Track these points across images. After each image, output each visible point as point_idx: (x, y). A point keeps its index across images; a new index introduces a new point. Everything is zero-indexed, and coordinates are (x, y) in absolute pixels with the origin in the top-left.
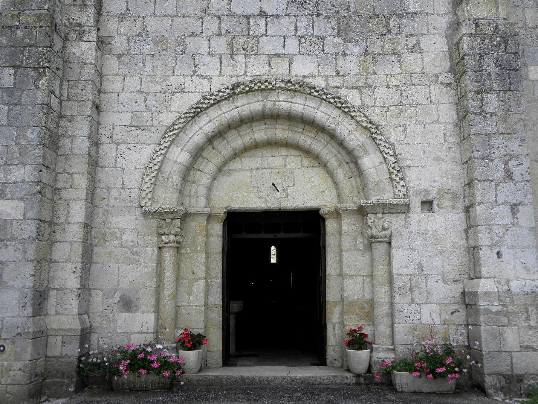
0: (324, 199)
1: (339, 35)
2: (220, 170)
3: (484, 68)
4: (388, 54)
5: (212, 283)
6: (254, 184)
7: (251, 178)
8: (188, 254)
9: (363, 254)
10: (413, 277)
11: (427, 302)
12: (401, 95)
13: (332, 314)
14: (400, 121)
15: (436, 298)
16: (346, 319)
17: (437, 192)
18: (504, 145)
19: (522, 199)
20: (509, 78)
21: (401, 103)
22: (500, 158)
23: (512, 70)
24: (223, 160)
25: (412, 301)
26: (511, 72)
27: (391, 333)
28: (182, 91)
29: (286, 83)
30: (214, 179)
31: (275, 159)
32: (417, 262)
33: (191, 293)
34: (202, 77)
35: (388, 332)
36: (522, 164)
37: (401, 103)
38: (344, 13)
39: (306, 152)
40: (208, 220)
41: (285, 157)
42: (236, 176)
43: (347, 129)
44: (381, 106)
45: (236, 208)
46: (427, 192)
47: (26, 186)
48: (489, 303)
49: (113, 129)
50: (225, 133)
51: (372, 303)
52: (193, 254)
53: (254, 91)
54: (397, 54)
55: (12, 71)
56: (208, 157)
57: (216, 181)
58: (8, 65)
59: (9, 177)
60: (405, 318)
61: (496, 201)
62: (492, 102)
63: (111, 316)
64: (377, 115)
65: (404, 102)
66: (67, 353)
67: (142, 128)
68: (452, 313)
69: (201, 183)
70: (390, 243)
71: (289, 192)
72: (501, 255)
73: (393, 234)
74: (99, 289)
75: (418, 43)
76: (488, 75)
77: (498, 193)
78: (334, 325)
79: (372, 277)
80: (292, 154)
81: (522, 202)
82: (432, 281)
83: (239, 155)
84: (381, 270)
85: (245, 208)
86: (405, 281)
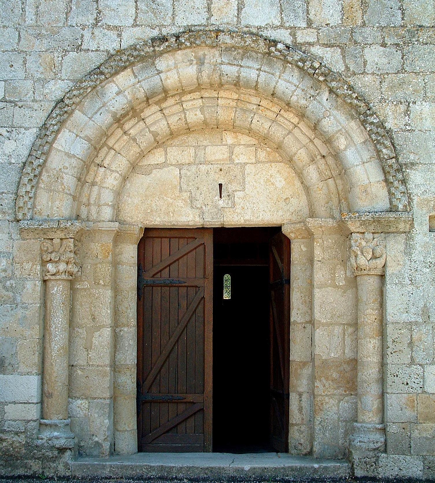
2: (134, 167)
6: (184, 187)
7: (181, 178)
8: (85, 290)
10: (414, 327)
12: (402, 58)
14: (400, 94)
25: (413, 361)
27: (380, 406)
28: (78, 48)
30: (125, 179)
34: (109, 27)
37: (403, 70)
39: (264, 139)
41: (231, 148)
44: (373, 74)
45: (157, 223)
51: (354, 363)
53: (184, 49)
56: (116, 147)
60: (401, 386)
64: (365, 83)
67: (20, 104)
70: (382, 277)
73: (388, 264)
79: (355, 325)
84: (370, 315)
85: (170, 222)
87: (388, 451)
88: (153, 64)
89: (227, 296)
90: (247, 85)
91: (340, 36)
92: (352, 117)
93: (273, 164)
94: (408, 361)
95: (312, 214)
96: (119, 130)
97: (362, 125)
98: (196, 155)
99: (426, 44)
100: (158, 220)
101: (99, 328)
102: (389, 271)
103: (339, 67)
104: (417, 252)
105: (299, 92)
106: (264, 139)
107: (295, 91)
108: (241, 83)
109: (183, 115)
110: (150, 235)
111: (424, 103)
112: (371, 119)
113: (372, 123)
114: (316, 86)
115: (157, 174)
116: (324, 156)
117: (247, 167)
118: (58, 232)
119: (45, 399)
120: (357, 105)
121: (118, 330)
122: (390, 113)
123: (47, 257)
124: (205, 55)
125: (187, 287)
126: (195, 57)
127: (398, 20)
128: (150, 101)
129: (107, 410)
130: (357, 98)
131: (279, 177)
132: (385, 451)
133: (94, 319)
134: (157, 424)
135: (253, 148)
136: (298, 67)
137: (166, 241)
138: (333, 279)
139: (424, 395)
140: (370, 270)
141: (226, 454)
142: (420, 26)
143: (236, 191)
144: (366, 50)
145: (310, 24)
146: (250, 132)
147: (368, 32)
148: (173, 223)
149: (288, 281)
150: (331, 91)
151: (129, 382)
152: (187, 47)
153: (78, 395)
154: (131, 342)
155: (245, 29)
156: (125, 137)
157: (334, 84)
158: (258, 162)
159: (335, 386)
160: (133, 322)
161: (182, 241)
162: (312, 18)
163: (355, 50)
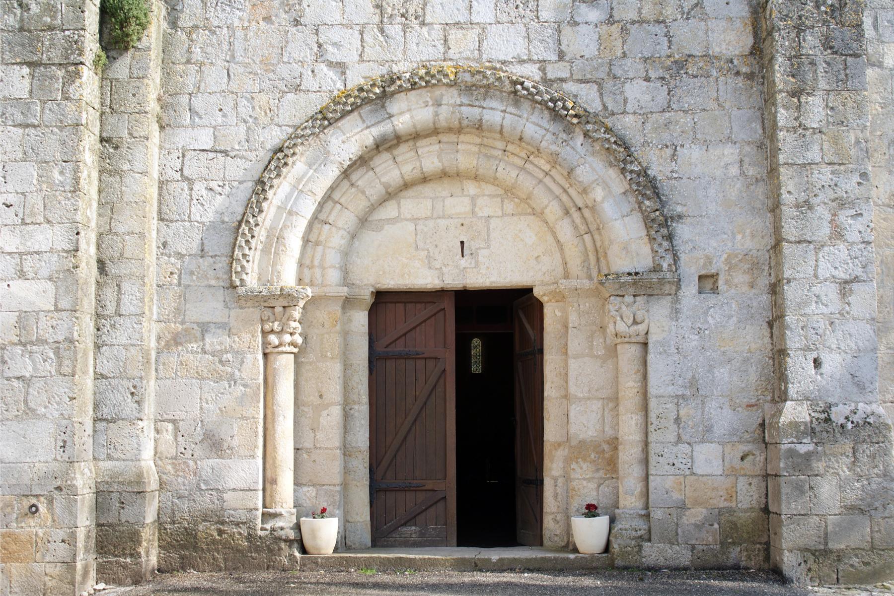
0: (540, 270)
2: (364, 221)
3: (804, 51)
4: (648, 22)
5: (352, 412)
6: (421, 244)
7: (416, 234)
8: (311, 363)
9: (604, 362)
10: (681, 401)
11: (703, 442)
12: (669, 94)
13: (552, 461)
15: (720, 430)
16: (573, 469)
17: (726, 260)
18: (832, 183)
19: (859, 272)
20: (845, 69)
21: (668, 108)
22: (825, 203)
23: (851, 55)
24: (368, 204)
25: (679, 440)
26: (849, 59)
27: (644, 490)
28: (297, 88)
29: (473, 75)
30: (353, 236)
31: (456, 202)
32: (689, 375)
33: (318, 428)
35: (639, 488)
36: (861, 214)
37: (668, 108)
39: (509, 191)
40: (344, 308)
41: (473, 199)
42: (390, 230)
43: (577, 152)
44: (635, 113)
45: (390, 286)
46: (709, 260)
47: (55, 258)
48: (795, 440)
49: (184, 156)
50: (371, 159)
51: (614, 443)
52: (320, 365)
53: (419, 88)
54: (664, 22)
55: (26, 70)
56: (342, 201)
57: (355, 240)
58: (18, 61)
59: (29, 244)
60: (667, 467)
61: (816, 276)
62: (816, 109)
63: (191, 463)
64: (627, 124)
65: (674, 106)
66: (128, 519)
67: (232, 154)
68: (742, 459)
69: (330, 245)
70: (645, 344)
71: (481, 259)
72: (820, 364)
73: (651, 331)
74: (169, 421)
76: (810, 63)
77: (820, 263)
78: (556, 480)
79: (614, 400)
80: (487, 193)
81: (857, 277)
82: (712, 405)
83: (396, 194)
84: (630, 386)
85: (406, 285)
86: (668, 406)
87: (652, 539)
88: (383, 106)
89: (476, 368)
90: (491, 129)
91: (597, 69)
92: (611, 165)
93: (522, 218)
94: (672, 437)
95: (567, 276)
96: (346, 181)
97: (622, 173)
98: (433, 207)
99: (696, 77)
100: (392, 282)
101: (326, 407)
102: (652, 339)
103: (595, 106)
104: (684, 317)
105: (549, 136)
107: (545, 135)
108: (484, 127)
109: (418, 164)
110: (383, 300)
111: (693, 145)
112: (629, 167)
113: (631, 172)
114: (569, 129)
115: (389, 230)
116: (580, 209)
117: (492, 221)
118: (281, 299)
119: (268, 486)
120: (616, 150)
121: (348, 408)
122: (654, 159)
123: (267, 327)
124: (442, 95)
125: (426, 359)
126: (431, 98)
127: (664, 50)
128: (381, 149)
129: (337, 498)
130: (615, 142)
131: (528, 232)
132: (649, 540)
133: (321, 396)
134: (391, 515)
135: (499, 199)
136: (548, 108)
137: (400, 306)
138: (591, 347)
139: (693, 478)
140: (630, 337)
141: (471, 548)
142: (689, 56)
143: (480, 248)
144: (627, 86)
146: (494, 181)
147: (629, 64)
148: (409, 286)
150: (586, 135)
151: (361, 467)
152: (421, 87)
153: (304, 482)
154: (363, 422)
155: (487, 64)
156: (353, 190)
157: (589, 127)
158: (504, 215)
159: (594, 468)
160: (365, 399)
161: (419, 306)
162: (564, 49)
163: (614, 85)
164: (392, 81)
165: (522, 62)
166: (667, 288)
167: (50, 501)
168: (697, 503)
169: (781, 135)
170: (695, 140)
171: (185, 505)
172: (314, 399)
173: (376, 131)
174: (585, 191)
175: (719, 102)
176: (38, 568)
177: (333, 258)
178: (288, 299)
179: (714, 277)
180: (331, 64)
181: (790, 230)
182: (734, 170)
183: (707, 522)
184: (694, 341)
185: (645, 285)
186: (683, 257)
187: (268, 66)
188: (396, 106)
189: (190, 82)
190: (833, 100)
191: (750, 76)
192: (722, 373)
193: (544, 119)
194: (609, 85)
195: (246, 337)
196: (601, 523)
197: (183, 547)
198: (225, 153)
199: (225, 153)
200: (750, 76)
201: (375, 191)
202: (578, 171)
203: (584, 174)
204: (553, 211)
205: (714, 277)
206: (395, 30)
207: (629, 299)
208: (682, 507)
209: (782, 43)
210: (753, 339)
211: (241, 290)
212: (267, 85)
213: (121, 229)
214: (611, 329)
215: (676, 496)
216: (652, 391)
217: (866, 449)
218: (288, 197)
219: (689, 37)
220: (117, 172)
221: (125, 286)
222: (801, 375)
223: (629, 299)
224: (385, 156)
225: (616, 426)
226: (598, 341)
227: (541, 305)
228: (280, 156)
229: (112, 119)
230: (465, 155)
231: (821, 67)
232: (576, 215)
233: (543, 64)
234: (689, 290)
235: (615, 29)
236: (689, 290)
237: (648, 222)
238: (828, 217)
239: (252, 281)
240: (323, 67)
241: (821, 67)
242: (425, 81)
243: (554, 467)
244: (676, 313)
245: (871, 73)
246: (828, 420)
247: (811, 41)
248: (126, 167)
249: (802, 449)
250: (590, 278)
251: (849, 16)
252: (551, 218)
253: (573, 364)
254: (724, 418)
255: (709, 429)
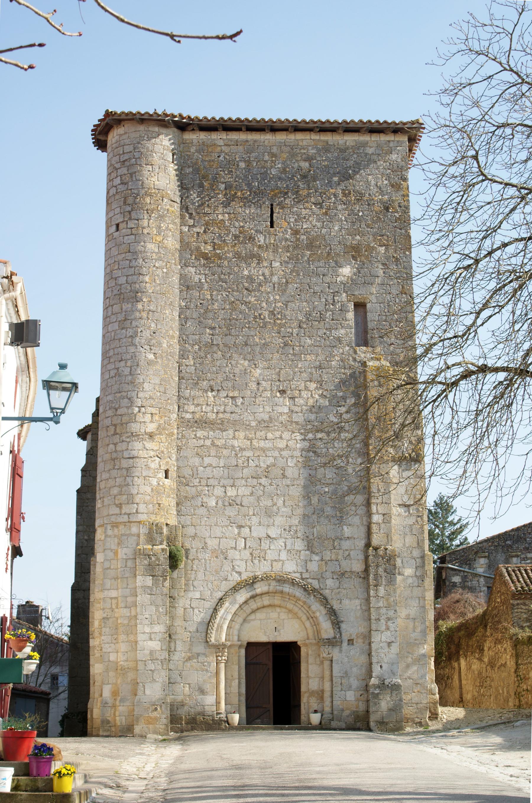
1: (308, 550)
2: (245, 620)
14: (338, 596)
19: (393, 640)
21: (339, 588)
25: (342, 690)
28: (226, 580)
31: (274, 614)
35: (330, 705)
37: (339, 588)
38: (311, 537)
39: (290, 611)
41: (279, 613)
46: (351, 635)
50: (55, 389)
51: (323, 691)
55: (151, 578)
62: (382, 591)
64: (327, 592)
70: (332, 661)
75: (349, 555)
79: (322, 678)
82: (351, 679)
84: (327, 673)
90: (285, 593)
94: (340, 689)
95: (308, 639)
100: (253, 640)
102: (334, 659)
103: (317, 587)
106: (290, 611)
110: (251, 647)
114: (309, 594)
145: (307, 571)
146: (286, 608)
149: (300, 662)
150: (314, 596)
160: (244, 677)
164: (256, 578)
165: (295, 572)
166: (338, 644)
167: (161, 707)
168: (347, 709)
169: (371, 598)
170: (347, 598)
171: (193, 710)
172: (230, 677)
173: (250, 594)
174: (314, 613)
175: (353, 585)
176: (157, 726)
177: (236, 632)
178: (224, 646)
179: (352, 640)
180: (236, 572)
181: (374, 627)
182: (359, 607)
183: (350, 715)
184: (346, 660)
185: (332, 642)
186: (343, 634)
187: (217, 572)
188: (256, 586)
189: (193, 577)
190: (387, 588)
191: (364, 578)
192: (355, 670)
193: (302, 591)
194: (321, 580)
195: (211, 658)
196: (318, 715)
197: (192, 723)
198: (204, 600)
199: (204, 600)
200: (364, 578)
201: (249, 611)
202: (312, 607)
203: (314, 608)
204: (304, 618)
205: (352, 640)
206: (256, 562)
207: (327, 647)
208: (343, 710)
209: (372, 570)
210: (363, 659)
211: (210, 643)
212: (217, 578)
213: (176, 624)
214: (321, 656)
215: (341, 707)
216: (334, 675)
217: (395, 693)
218: (224, 614)
219: (346, 565)
220: (174, 607)
221: (177, 642)
222: (376, 670)
223: (327, 647)
224: (252, 600)
225: (323, 686)
226: (318, 659)
227: (300, 647)
228: (221, 600)
229: (172, 591)
230: (277, 600)
231: (384, 578)
232: (311, 620)
233: (301, 573)
234: (345, 644)
235: (323, 563)
236: (345, 644)
237: (333, 623)
238: (385, 623)
239: (213, 640)
240: (235, 573)
241: (384, 578)
242: (266, 578)
243: (304, 699)
244: (341, 651)
245: (399, 578)
246: (384, 684)
247: (381, 570)
248: (177, 605)
249: (376, 692)
250: (315, 639)
251: (392, 562)
252: (303, 620)
253: (310, 666)
254: (355, 683)
255: (351, 687)
